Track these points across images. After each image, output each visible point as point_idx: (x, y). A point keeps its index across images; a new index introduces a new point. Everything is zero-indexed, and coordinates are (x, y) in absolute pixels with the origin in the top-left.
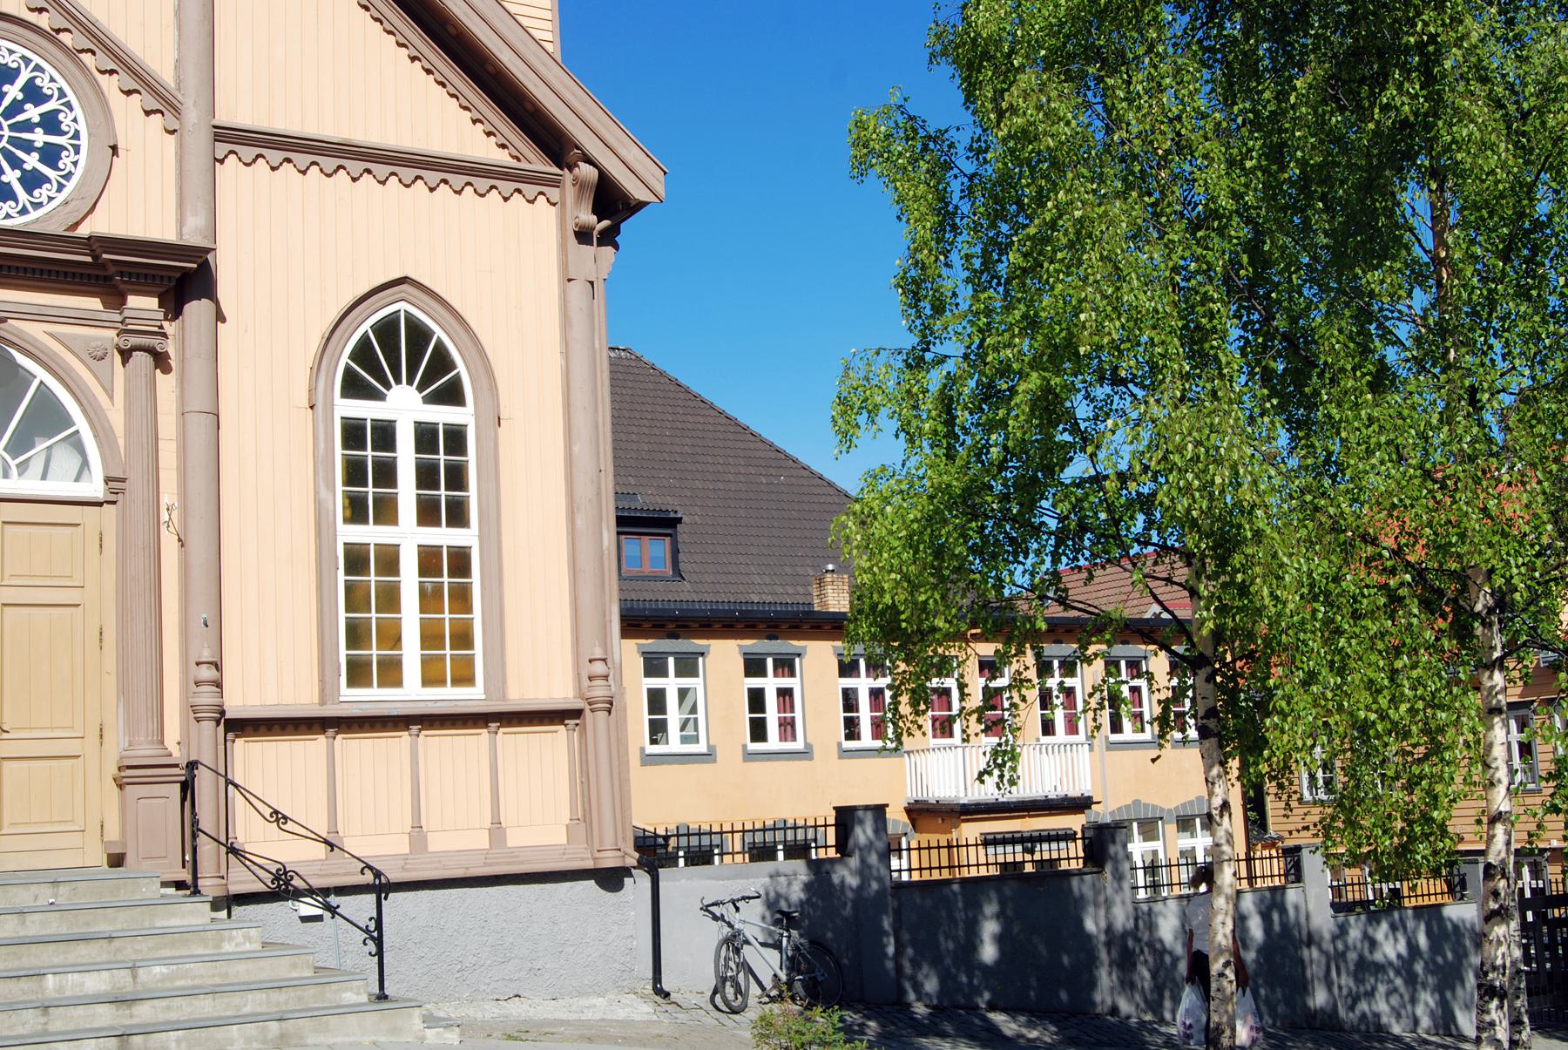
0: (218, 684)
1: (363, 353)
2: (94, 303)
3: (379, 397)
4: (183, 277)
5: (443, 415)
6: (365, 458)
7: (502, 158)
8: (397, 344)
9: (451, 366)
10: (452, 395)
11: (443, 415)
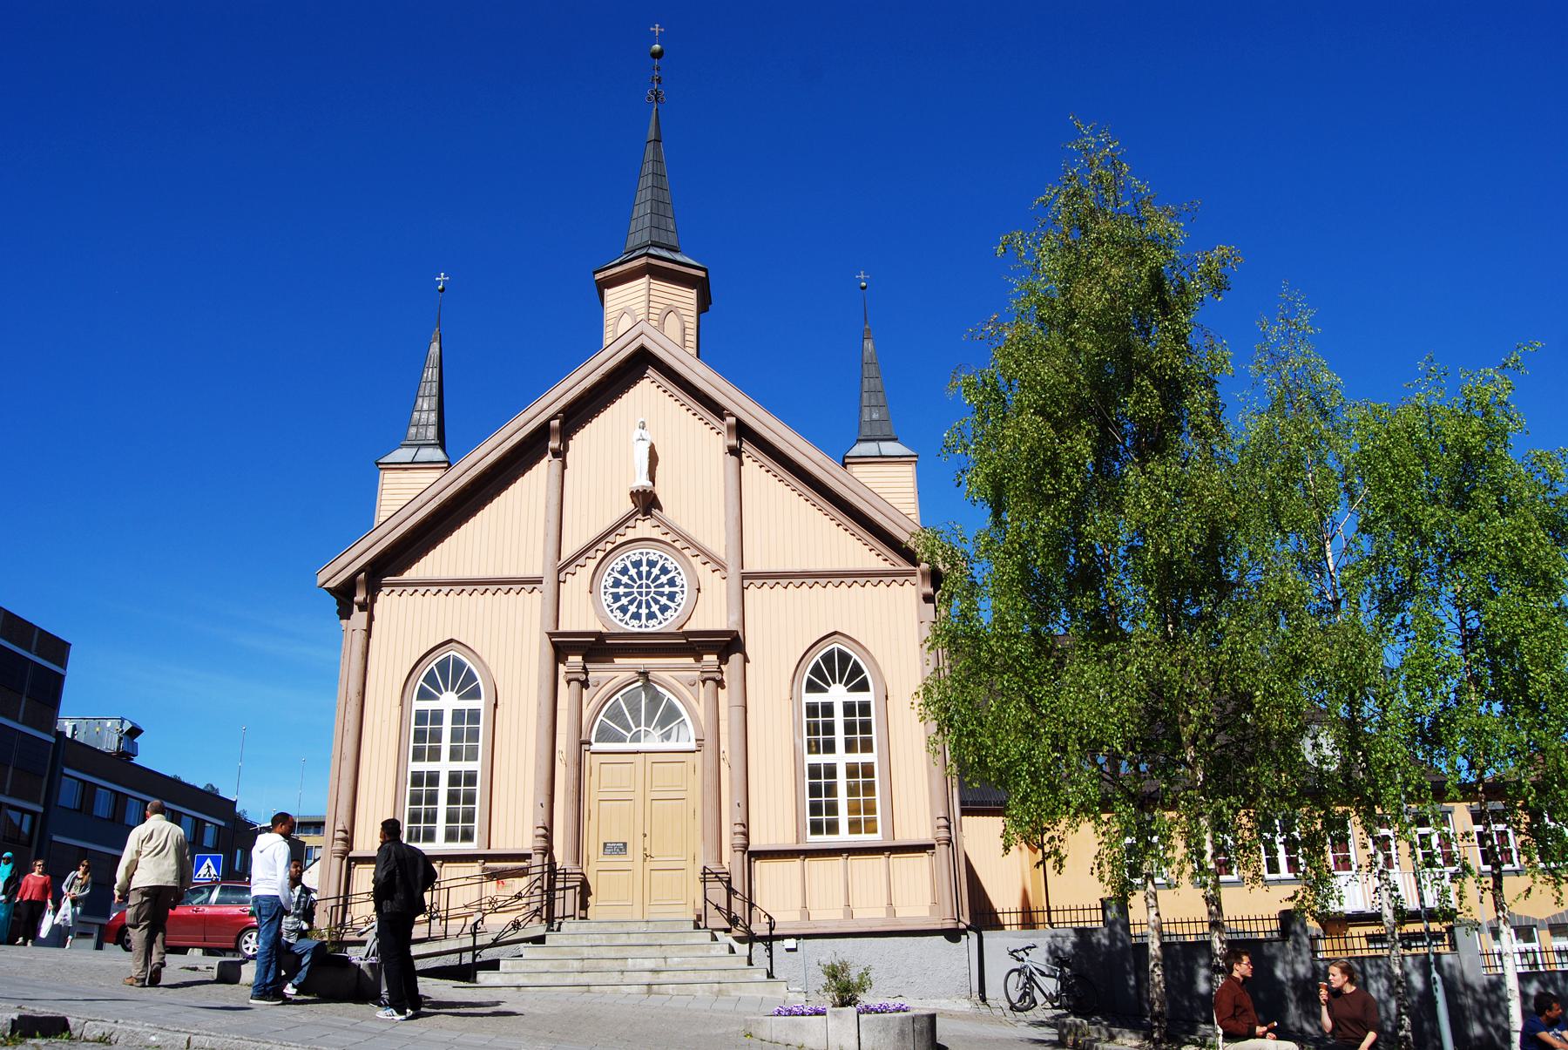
0: (948, 828)
1: (816, 670)
2: (691, 660)
3: (825, 691)
4: (729, 644)
5: (858, 697)
6: (818, 723)
7: (886, 566)
8: (836, 664)
9: (464, 665)
10: (863, 686)
11: (858, 697)
